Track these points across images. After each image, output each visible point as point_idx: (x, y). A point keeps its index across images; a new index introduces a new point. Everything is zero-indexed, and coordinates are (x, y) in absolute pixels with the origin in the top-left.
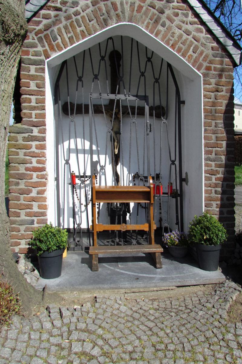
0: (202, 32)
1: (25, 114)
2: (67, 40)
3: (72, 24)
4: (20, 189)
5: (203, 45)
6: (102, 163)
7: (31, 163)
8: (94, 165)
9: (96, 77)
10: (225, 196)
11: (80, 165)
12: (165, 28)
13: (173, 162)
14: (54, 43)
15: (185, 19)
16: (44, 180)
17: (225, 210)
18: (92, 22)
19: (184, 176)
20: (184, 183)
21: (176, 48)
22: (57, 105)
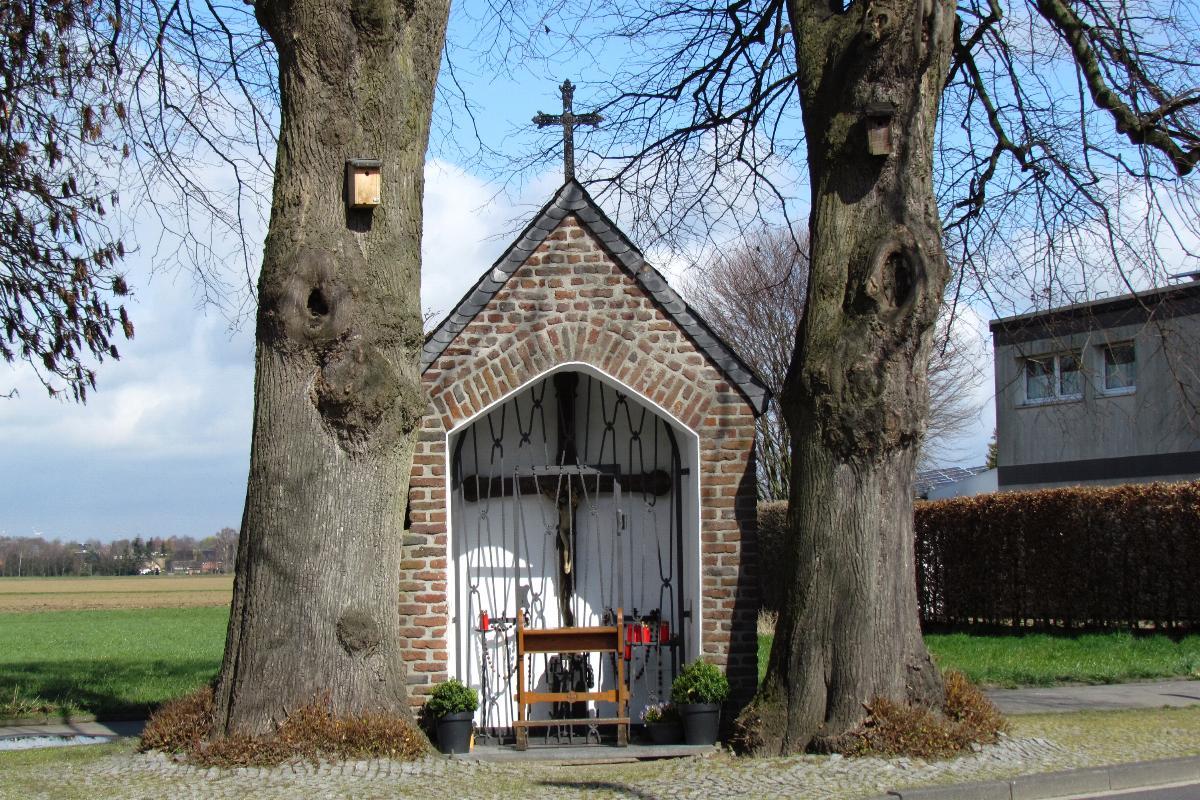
0: (699, 363)
1: (415, 515)
2: (479, 398)
3: (485, 373)
4: (407, 630)
5: (701, 384)
6: (537, 589)
7: (424, 589)
8: (521, 593)
9: (526, 438)
10: (740, 634)
11: (498, 597)
12: (636, 364)
13: (667, 583)
14: (459, 406)
15: (669, 345)
16: (443, 615)
17: (739, 656)
18: (517, 367)
19: (686, 609)
20: (686, 620)
21: (655, 395)
22: (457, 491)
